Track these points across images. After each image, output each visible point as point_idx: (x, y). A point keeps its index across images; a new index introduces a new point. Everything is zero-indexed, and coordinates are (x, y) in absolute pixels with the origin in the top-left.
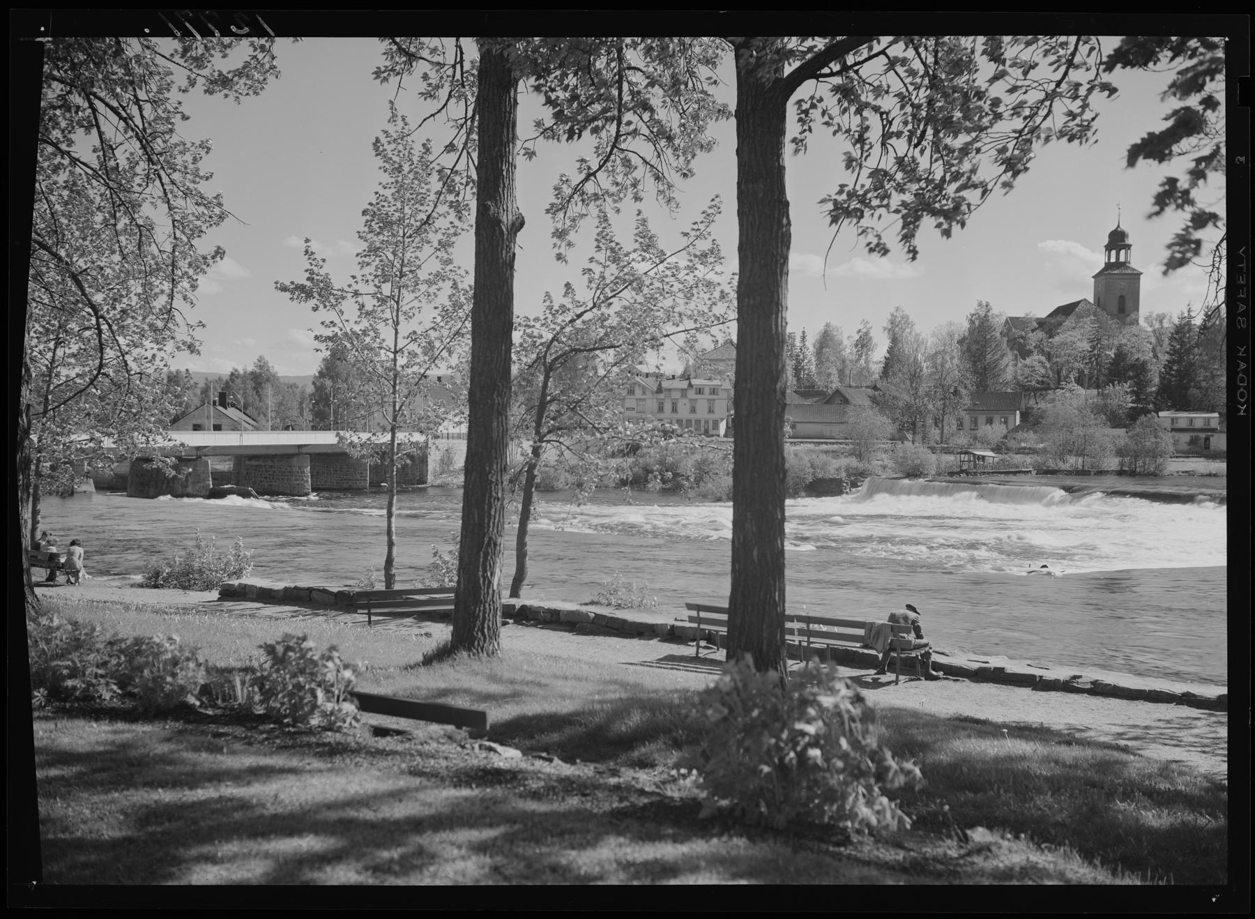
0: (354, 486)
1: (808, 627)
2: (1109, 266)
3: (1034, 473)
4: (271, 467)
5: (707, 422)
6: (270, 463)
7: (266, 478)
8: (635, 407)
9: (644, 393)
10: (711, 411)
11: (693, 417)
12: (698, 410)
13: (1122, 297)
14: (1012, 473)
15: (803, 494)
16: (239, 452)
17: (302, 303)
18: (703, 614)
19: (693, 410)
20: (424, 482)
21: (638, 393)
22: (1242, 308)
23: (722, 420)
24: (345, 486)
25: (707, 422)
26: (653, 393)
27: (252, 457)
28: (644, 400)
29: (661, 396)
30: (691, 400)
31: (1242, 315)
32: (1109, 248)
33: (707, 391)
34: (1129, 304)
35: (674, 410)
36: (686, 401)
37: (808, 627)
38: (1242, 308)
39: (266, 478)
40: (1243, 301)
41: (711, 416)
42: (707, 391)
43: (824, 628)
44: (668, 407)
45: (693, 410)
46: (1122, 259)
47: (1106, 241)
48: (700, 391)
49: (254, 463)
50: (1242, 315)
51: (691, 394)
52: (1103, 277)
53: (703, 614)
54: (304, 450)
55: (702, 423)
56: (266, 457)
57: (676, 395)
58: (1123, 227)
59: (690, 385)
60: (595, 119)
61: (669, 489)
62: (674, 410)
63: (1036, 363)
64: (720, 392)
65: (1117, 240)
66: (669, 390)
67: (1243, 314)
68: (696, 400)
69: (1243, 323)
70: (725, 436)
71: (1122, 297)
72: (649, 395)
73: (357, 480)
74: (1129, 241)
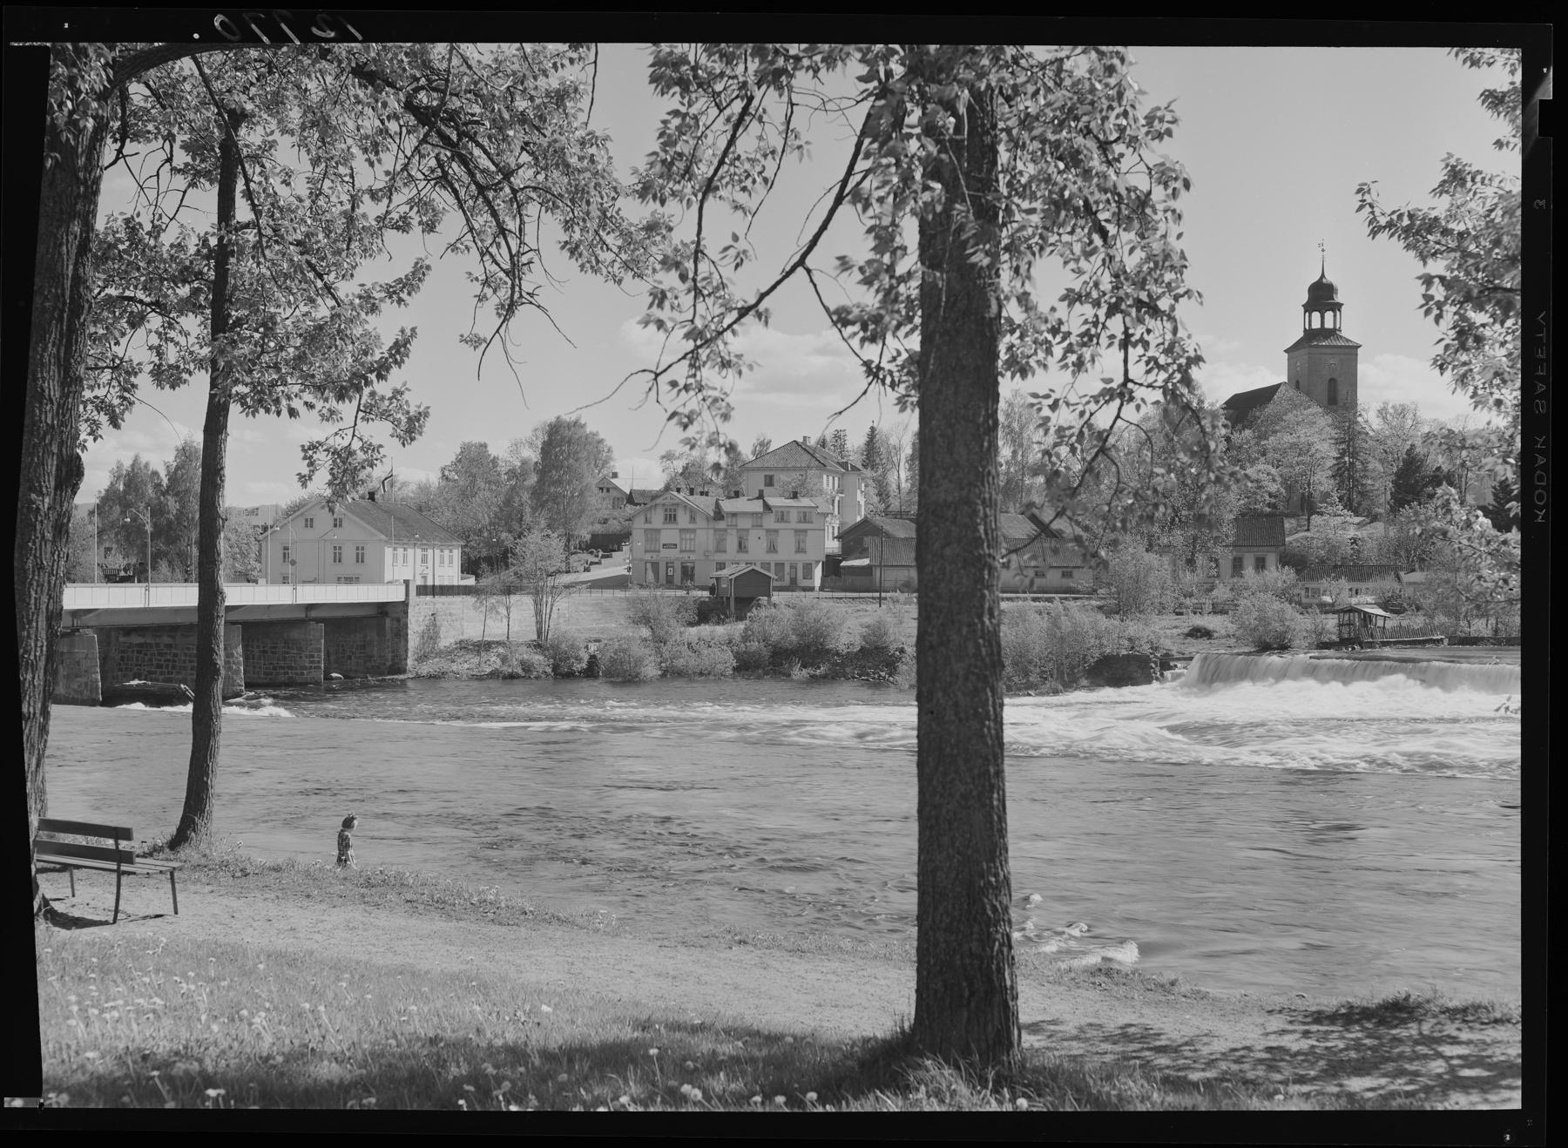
0: (299, 679)
1: (117, 845)
2: (1310, 335)
3: (1446, 642)
4: (169, 646)
5: (793, 567)
6: (166, 640)
7: (159, 666)
8: (677, 542)
9: (693, 519)
10: (800, 550)
11: (773, 558)
12: (780, 547)
13: (1332, 381)
14: (1420, 642)
15: (1084, 682)
16: (107, 621)
17: (1191, 279)
18: (109, 843)
19: (772, 549)
20: (404, 671)
21: (683, 519)
22: (1541, 388)
23: (818, 562)
24: (282, 678)
25: (793, 567)
26: (708, 518)
27: (128, 631)
28: (694, 531)
29: (722, 525)
30: (768, 531)
31: (1541, 396)
32: (1309, 308)
33: (794, 516)
34: (1342, 391)
35: (742, 547)
36: (762, 533)
37: (117, 845)
38: (1541, 388)
39: (159, 666)
40: (1543, 380)
41: (800, 557)
42: (794, 516)
43: (80, 840)
44: (732, 542)
45: (772, 549)
46: (1329, 324)
47: (1305, 298)
48: (782, 518)
49: (136, 639)
50: (1541, 396)
51: (770, 521)
52: (1303, 351)
53: (109, 843)
54: (313, 614)
55: (787, 569)
56: (157, 630)
57: (744, 523)
58: (1330, 278)
59: (767, 507)
60: (465, 161)
61: (825, 677)
62: (742, 547)
63: (1262, 476)
64: (814, 518)
65: (1322, 296)
66: (734, 515)
67: (1542, 396)
68: (776, 531)
69: (1542, 407)
70: (822, 589)
71: (1332, 381)
72: (701, 522)
73: (305, 668)
74: (1339, 298)
